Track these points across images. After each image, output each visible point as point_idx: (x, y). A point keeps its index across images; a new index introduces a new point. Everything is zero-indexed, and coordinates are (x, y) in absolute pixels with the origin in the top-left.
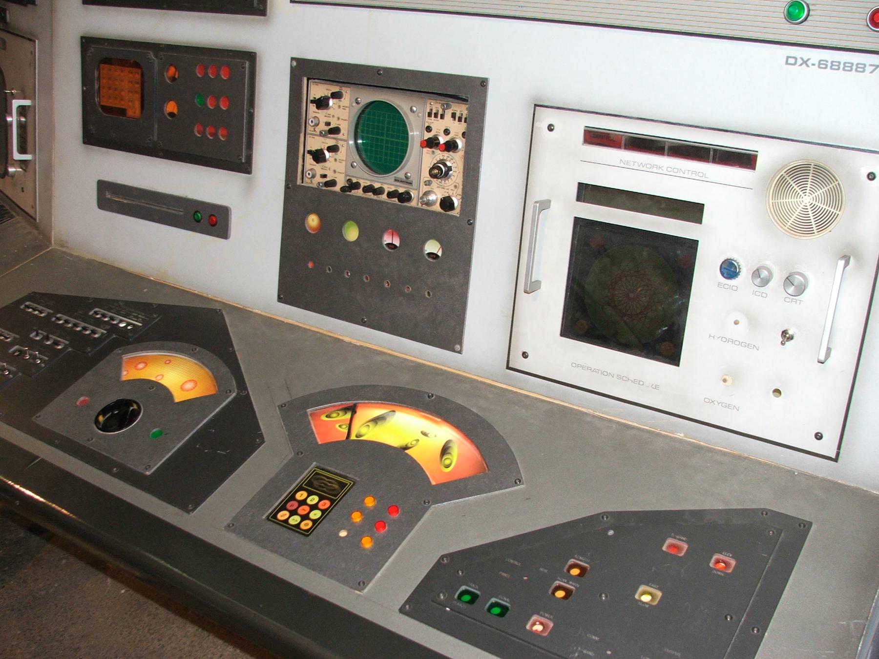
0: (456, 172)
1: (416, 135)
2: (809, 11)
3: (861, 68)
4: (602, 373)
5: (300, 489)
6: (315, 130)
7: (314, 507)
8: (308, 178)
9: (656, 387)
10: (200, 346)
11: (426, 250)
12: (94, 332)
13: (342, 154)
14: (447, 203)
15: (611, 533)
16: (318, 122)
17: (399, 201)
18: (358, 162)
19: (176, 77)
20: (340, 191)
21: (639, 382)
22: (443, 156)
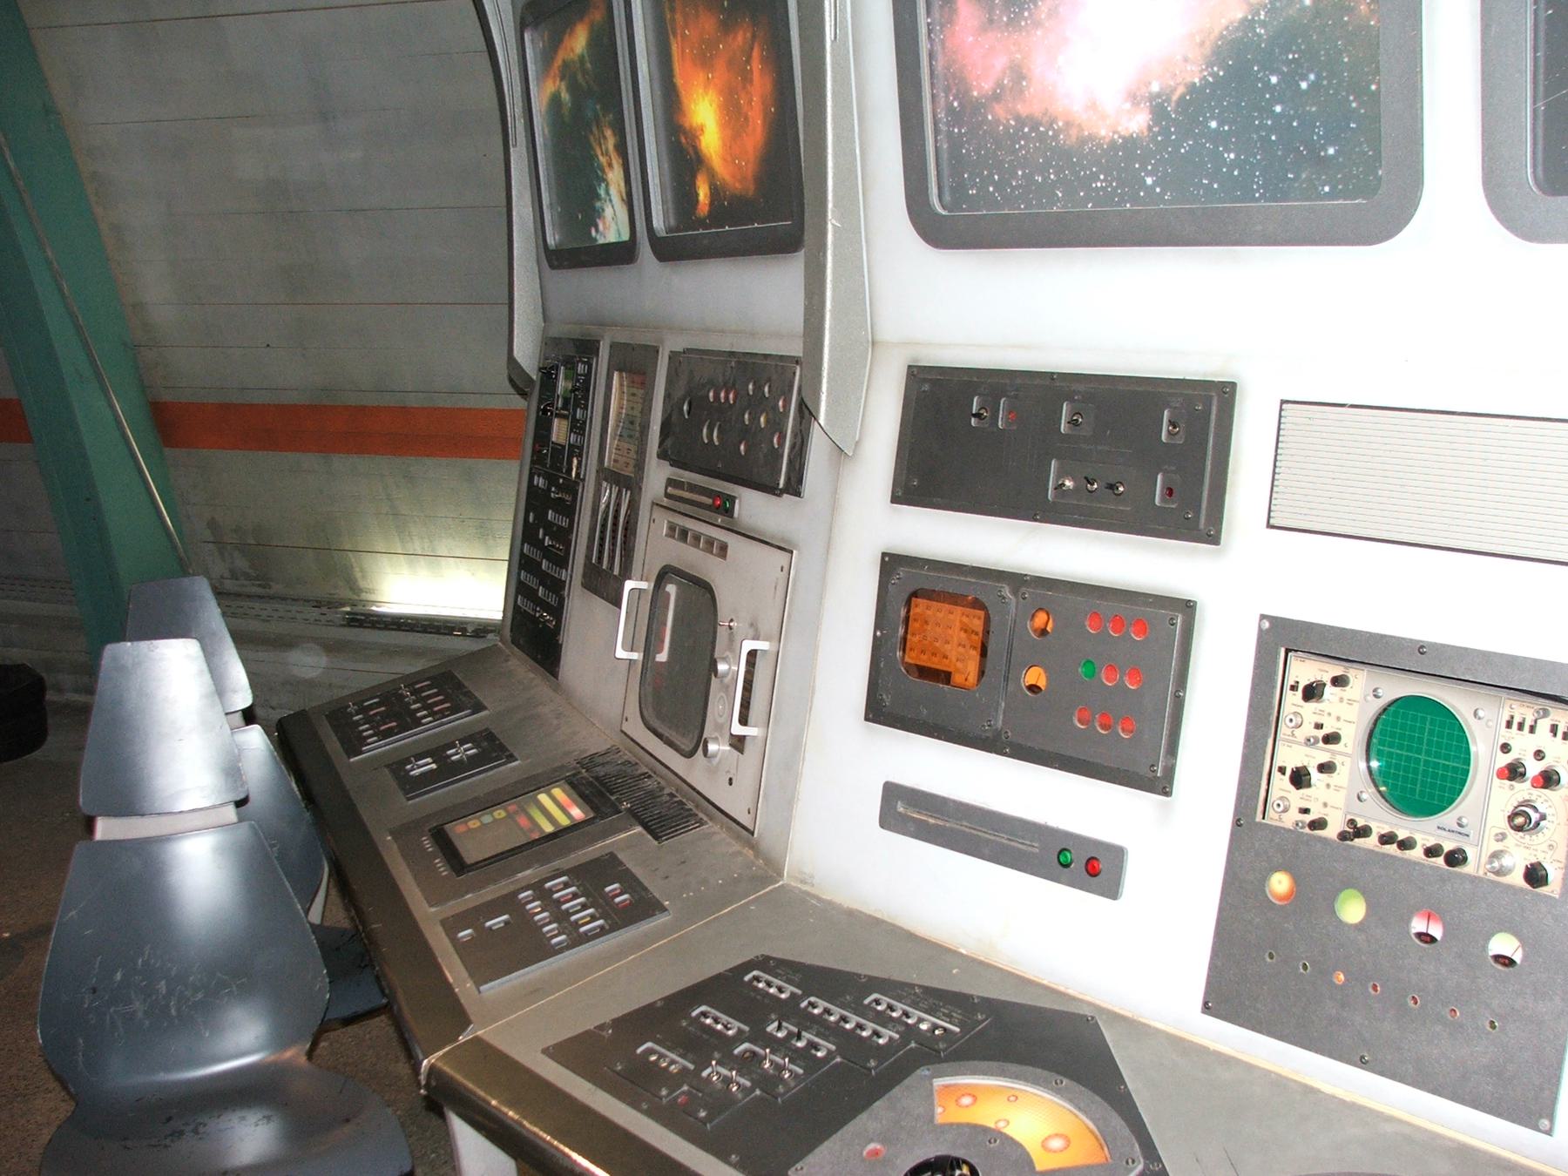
0: (1553, 822)
1: (1484, 756)
6: (1293, 735)
8: (1276, 812)
10: (1071, 1078)
11: (1414, 928)
12: (876, 1034)
13: (1340, 777)
16: (1300, 723)
18: (1369, 793)
19: (1049, 629)
22: (1530, 794)
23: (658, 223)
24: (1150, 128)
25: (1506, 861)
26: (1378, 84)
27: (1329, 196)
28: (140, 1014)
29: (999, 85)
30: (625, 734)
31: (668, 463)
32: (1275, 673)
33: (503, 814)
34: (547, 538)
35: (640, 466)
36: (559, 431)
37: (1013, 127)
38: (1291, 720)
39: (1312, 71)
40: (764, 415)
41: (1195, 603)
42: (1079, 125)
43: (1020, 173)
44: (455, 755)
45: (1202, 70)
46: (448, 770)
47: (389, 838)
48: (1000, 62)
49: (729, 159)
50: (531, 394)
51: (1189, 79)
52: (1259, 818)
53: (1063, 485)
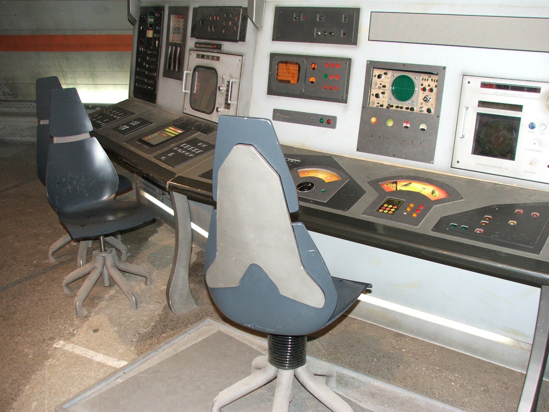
1: (418, 89)
4: (487, 165)
5: (384, 204)
6: (375, 87)
7: (391, 208)
13: (386, 95)
14: (429, 111)
15: (497, 209)
17: (411, 110)
19: (315, 68)
25: (423, 109)
28: (70, 190)
30: (185, 113)
32: (371, 73)
33: (157, 135)
35: (184, 40)
36: (150, 34)
40: (231, 22)
46: (132, 128)
47: (125, 143)
50: (135, 24)
52: (368, 106)
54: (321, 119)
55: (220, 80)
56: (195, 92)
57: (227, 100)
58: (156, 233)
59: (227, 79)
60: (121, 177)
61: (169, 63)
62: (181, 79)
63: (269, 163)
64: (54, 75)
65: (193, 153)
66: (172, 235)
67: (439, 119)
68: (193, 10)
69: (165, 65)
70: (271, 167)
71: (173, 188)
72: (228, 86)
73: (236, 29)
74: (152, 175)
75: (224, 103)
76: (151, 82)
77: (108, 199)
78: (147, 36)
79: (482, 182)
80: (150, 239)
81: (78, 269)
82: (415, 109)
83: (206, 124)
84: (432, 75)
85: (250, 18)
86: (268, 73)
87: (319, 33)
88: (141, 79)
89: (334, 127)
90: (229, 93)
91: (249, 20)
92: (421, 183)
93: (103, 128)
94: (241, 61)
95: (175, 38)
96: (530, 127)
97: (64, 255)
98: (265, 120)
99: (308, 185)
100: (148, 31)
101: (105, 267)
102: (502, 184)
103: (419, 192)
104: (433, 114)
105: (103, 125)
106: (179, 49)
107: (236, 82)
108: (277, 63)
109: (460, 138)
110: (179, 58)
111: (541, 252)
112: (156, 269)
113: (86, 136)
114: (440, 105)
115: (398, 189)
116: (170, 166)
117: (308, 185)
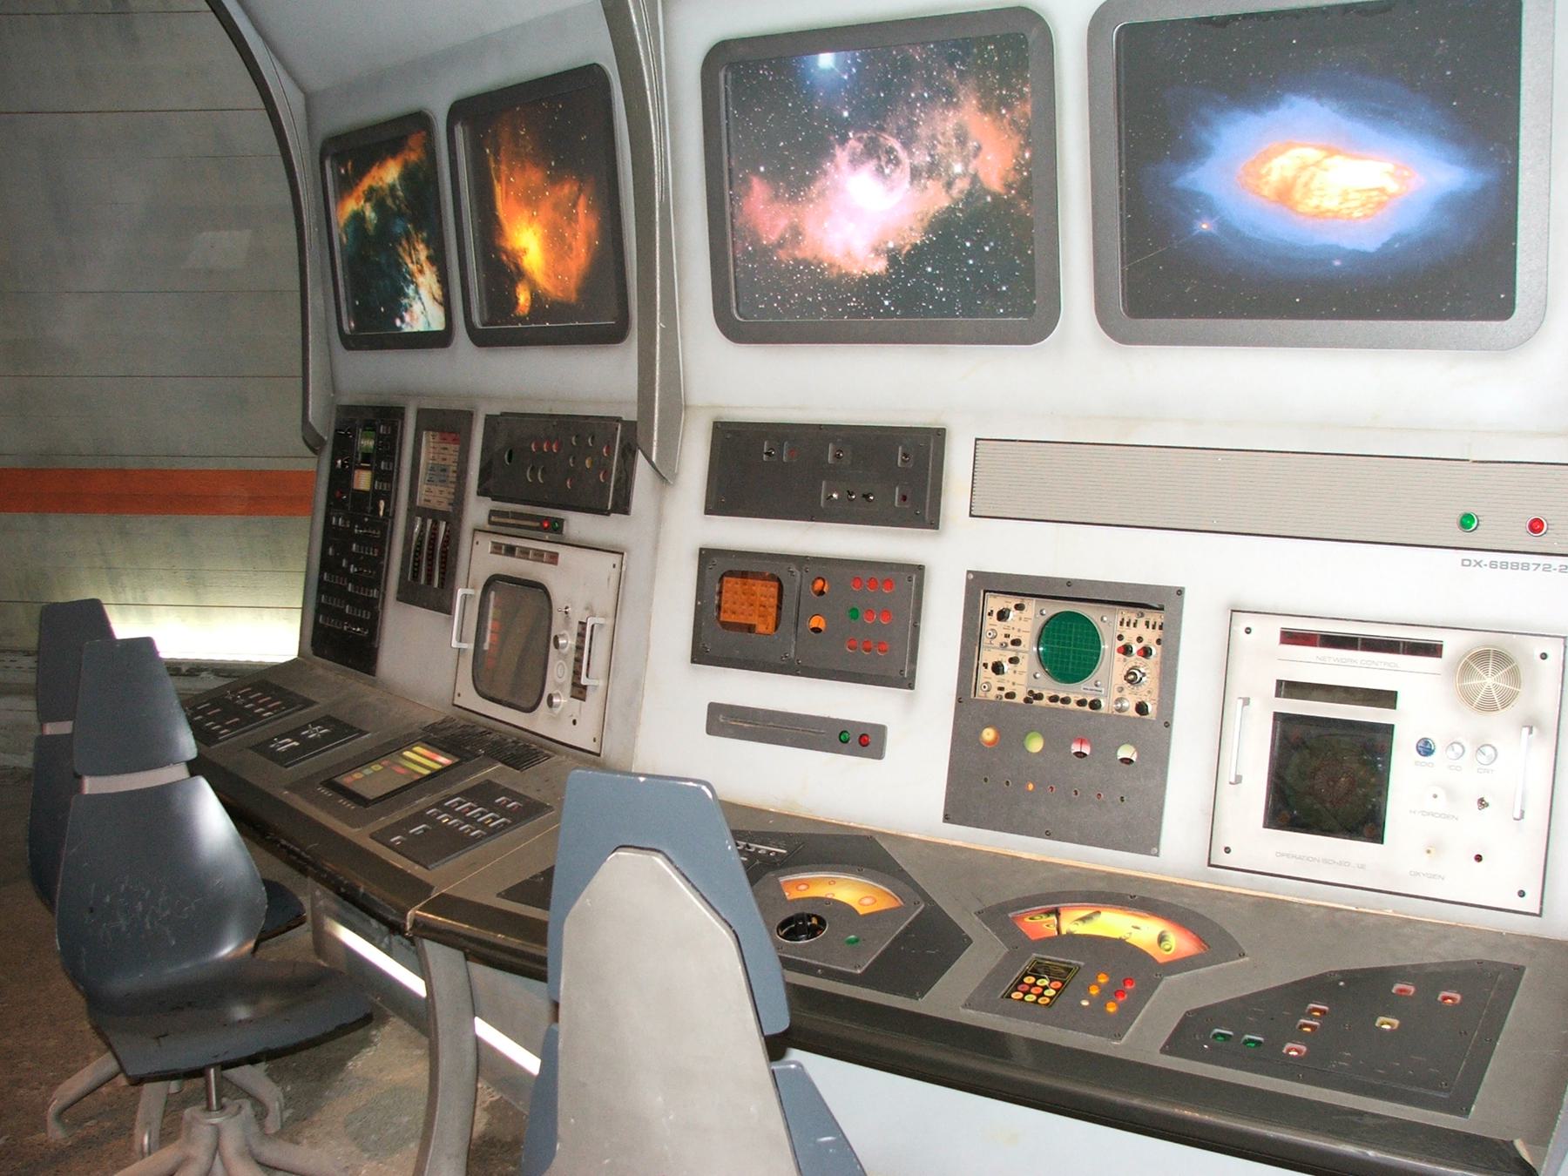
1: (1108, 646)
2: (1478, 521)
3: (1526, 567)
5: (1026, 975)
7: (1045, 988)
9: (1362, 867)
14: (1141, 708)
15: (1342, 984)
17: (1091, 708)
20: (1022, 702)
21: (1346, 864)
23: (476, 319)
24: (887, 270)
25: (1126, 704)
26: (1032, 250)
27: (1001, 315)
28: (124, 929)
29: (783, 238)
31: (489, 499)
32: (978, 607)
33: (380, 768)
34: (352, 566)
35: (459, 501)
37: (792, 265)
38: (990, 634)
39: (991, 241)
41: (924, 566)
42: (839, 266)
43: (796, 295)
44: (313, 734)
45: (922, 236)
46: (308, 747)
47: (286, 792)
48: (783, 223)
49: (552, 275)
51: (913, 241)
52: (972, 696)
53: (832, 496)
54: (842, 732)
55: (558, 618)
56: (486, 646)
57: (577, 673)
58: (370, 1046)
59: (577, 615)
60: (274, 889)
61: (416, 564)
62: (448, 610)
63: (708, 903)
64: (91, 594)
65: (483, 825)
66: (414, 1053)
67: (1170, 732)
68: (486, 420)
69: (403, 569)
70: (711, 911)
71: (425, 930)
72: (581, 635)
73: (604, 478)
74: (365, 889)
75: (569, 683)
76: (366, 615)
77: (232, 955)
78: (355, 487)
79: (1296, 906)
80: (350, 1064)
81: (137, 1164)
82: (1103, 704)
83: (519, 739)
84: (1147, 610)
85: (642, 451)
86: (694, 604)
87: (835, 496)
88: (335, 603)
89: (878, 754)
90: (582, 655)
91: (640, 456)
92: (1126, 910)
93: (222, 744)
94: (617, 566)
95: (434, 495)
96: (1419, 752)
97: (91, 1118)
98: (695, 785)
99: (809, 924)
100: (356, 472)
101: (217, 1157)
102: (1354, 909)
103: (1123, 938)
104: (1154, 719)
105: (223, 735)
106: (443, 526)
107: (602, 625)
108: (720, 576)
109: (1231, 783)
110: (442, 552)
111: (1473, 1109)
112: (369, 1158)
113: (178, 773)
114: (1173, 694)
115: (1064, 932)
116: (418, 863)
117: (809, 924)
